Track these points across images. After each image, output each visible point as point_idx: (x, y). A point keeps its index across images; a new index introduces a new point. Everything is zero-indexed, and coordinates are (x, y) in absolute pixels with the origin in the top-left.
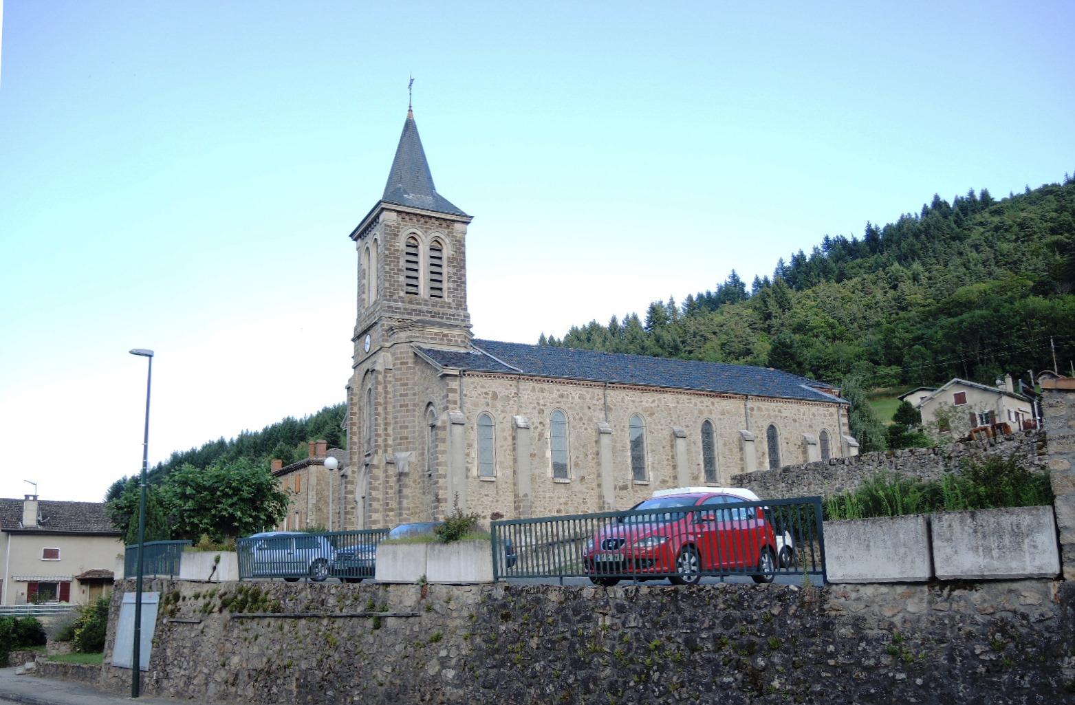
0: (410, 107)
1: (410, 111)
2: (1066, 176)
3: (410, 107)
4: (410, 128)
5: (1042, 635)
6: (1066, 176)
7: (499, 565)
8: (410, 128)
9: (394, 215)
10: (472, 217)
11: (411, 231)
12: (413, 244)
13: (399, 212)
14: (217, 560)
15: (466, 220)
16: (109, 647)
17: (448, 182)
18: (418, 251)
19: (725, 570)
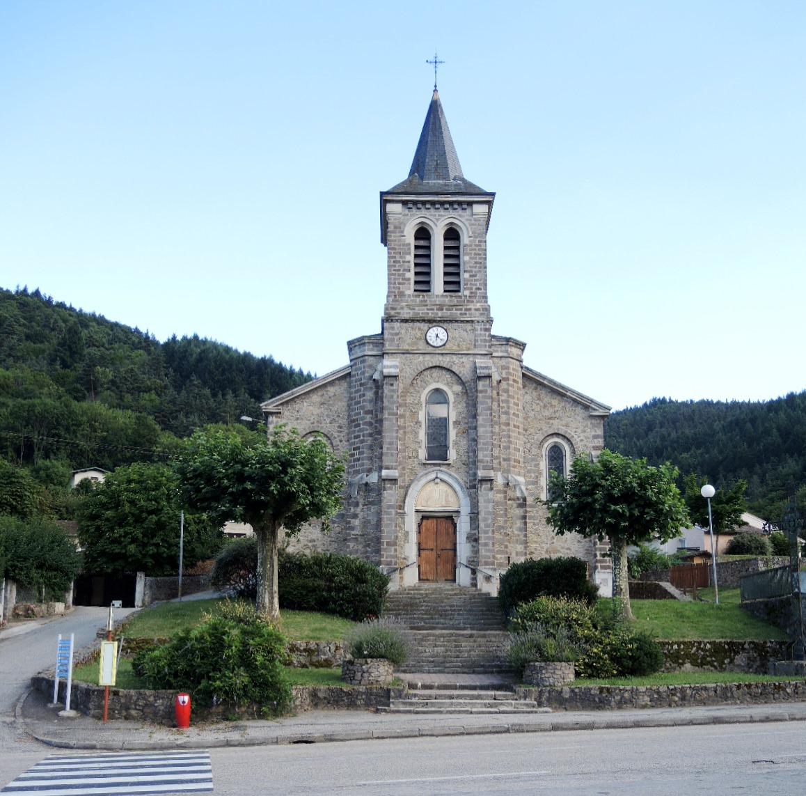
0: (436, 86)
1: (435, 91)
2: (18, 287)
3: (436, 86)
4: (434, 110)
5: (714, 417)
6: (18, 287)
7: (151, 752)
8: (434, 110)
9: (400, 205)
10: (493, 194)
11: (434, 217)
12: (423, 234)
13: (405, 203)
14: (432, 550)
15: (488, 199)
16: (332, 714)
17: (472, 161)
18: (430, 243)
19: (476, 540)
